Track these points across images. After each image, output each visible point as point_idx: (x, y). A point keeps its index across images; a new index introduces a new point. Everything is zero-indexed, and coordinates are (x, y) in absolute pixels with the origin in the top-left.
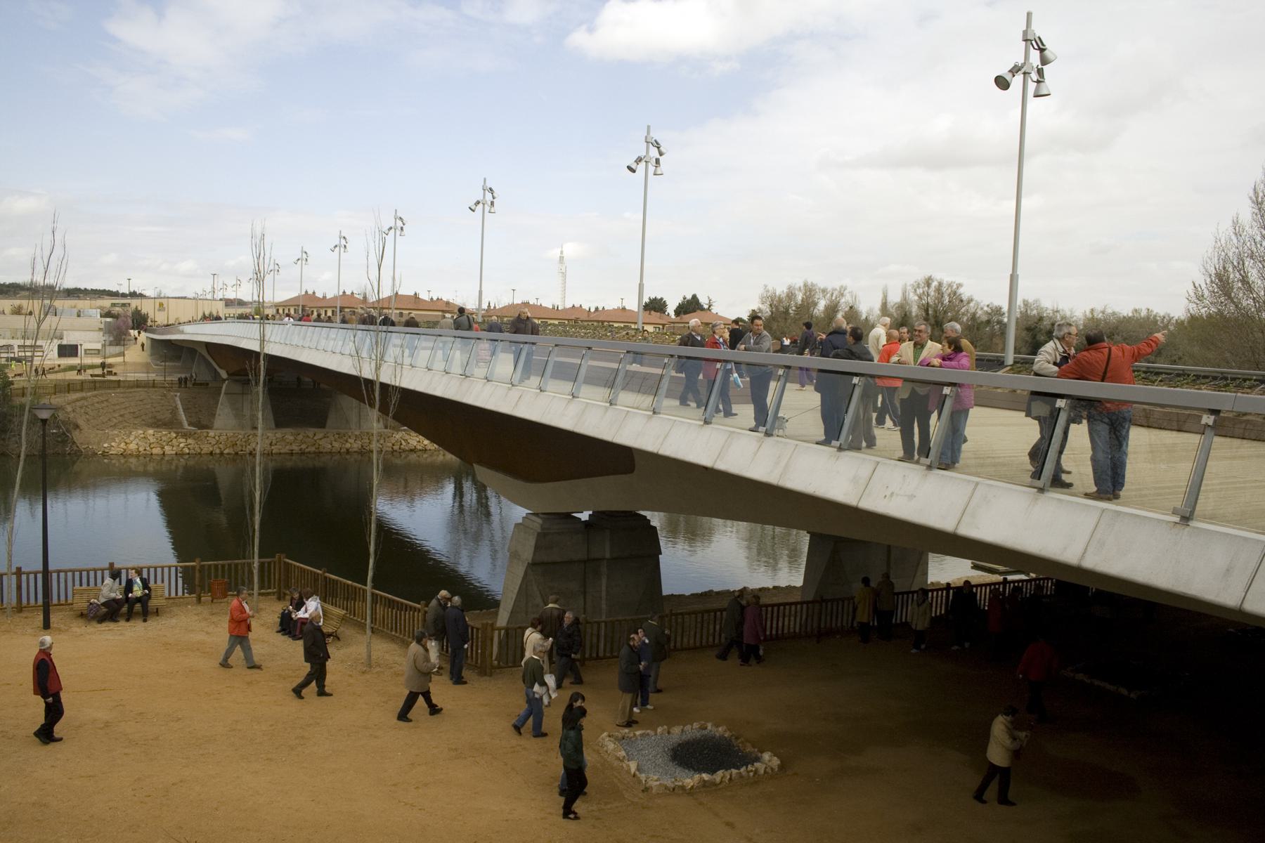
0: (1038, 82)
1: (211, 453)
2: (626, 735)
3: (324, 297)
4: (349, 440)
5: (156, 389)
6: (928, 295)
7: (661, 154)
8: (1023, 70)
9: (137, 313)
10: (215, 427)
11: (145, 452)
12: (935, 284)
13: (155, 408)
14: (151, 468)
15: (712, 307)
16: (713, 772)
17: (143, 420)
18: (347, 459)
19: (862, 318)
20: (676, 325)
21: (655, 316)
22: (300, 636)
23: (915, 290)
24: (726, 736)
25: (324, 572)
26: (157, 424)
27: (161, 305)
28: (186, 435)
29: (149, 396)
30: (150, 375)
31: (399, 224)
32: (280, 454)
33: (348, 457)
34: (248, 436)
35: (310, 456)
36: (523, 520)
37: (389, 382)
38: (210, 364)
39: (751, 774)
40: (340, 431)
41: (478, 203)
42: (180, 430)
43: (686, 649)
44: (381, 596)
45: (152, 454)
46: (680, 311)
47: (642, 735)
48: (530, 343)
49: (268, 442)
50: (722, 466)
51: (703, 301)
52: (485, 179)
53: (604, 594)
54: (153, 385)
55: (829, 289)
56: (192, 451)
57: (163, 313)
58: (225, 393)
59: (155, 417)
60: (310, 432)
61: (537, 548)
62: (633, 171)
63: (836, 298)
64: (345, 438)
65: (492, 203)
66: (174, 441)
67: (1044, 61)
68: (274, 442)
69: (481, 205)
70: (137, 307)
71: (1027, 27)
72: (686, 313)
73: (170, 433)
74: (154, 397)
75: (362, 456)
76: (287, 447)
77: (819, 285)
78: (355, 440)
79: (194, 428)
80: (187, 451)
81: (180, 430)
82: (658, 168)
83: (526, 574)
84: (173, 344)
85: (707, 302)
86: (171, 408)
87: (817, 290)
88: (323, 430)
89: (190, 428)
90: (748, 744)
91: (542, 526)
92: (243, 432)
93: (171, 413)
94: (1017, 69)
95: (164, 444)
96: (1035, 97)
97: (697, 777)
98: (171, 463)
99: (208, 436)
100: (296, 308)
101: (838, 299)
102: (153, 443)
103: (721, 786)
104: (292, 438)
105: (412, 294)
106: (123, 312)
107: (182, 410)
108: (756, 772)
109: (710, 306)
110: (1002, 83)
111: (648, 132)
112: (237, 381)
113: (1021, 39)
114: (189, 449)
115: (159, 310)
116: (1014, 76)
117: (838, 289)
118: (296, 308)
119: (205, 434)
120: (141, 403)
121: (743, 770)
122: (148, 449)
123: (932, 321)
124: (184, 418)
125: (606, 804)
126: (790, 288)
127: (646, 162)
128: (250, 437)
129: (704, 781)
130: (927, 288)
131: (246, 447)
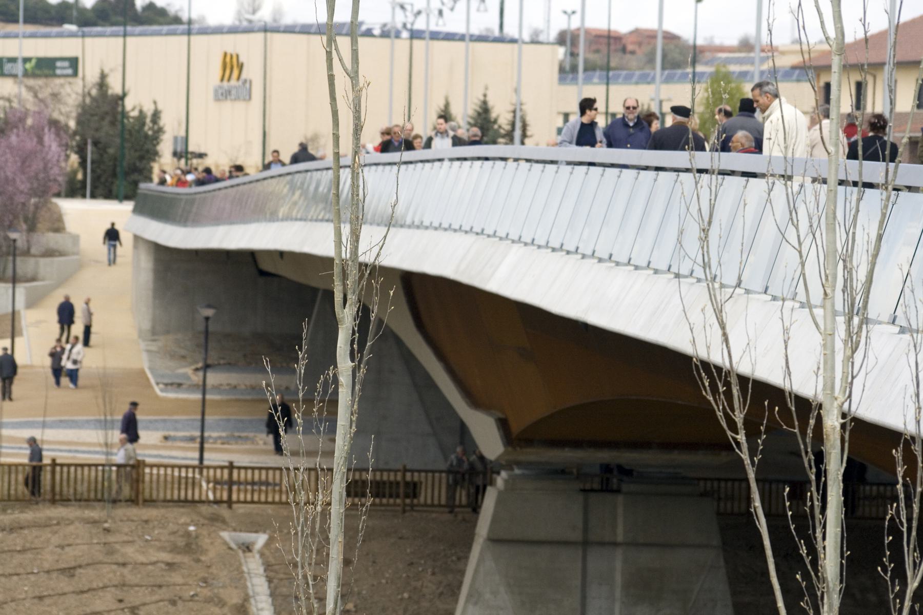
37: (687, 349)
38: (431, 385)
57: (240, 106)
58: (494, 540)
70: (103, 76)
74: (130, 552)
84: (263, 273)
106: (27, 96)
112: (560, 473)
115: (223, 95)
120: (64, 584)
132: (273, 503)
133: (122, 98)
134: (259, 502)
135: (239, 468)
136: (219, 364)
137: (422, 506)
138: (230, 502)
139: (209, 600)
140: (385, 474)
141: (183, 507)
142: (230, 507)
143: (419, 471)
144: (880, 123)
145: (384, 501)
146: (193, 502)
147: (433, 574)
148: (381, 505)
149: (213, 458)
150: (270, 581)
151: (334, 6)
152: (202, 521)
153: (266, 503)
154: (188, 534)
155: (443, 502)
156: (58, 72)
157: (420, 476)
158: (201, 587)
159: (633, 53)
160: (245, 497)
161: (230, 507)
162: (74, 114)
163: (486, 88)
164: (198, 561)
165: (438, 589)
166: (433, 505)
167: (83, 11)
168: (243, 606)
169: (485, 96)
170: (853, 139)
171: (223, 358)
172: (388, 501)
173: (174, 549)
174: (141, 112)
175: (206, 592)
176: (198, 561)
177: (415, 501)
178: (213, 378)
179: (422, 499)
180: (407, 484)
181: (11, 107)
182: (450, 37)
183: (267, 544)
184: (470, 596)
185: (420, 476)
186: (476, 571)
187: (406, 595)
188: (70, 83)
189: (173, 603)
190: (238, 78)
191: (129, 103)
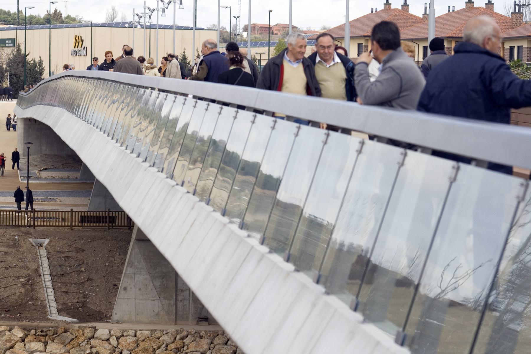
10: (115, 317)
19: (22, 53)
27: (79, 41)
34: (182, 339)
48: (219, 102)
57: (82, 58)
73: (10, 331)
79: (69, 319)
92: (172, 329)
93: (24, 285)
99: (93, 337)
107: (48, 277)
119: (88, 333)
124: (52, 297)
128: (186, 341)
132: (53, 226)
133: (25, 56)
134: (47, 226)
135: (38, 211)
136: (51, 168)
137: (117, 226)
138: (34, 226)
139: (22, 268)
140: (92, 213)
141: (14, 228)
142: (34, 228)
143: (115, 212)
144: (238, 58)
145: (101, 224)
146: (18, 226)
147: (120, 255)
148: (99, 226)
150: (49, 259)
152: (21, 234)
153: (50, 226)
154: (15, 240)
155: (126, 225)
156: (7, 45)
157: (115, 214)
158: (19, 262)
159: (276, 34)
160: (68, 224)
161: (34, 228)
162: (5, 63)
163: (185, 49)
164: (18, 251)
165: (121, 261)
166: (121, 226)
167: (39, 19)
168: (37, 269)
169: (184, 52)
171: (53, 166)
172: (93, 225)
173: (8, 246)
174: (34, 61)
175: (21, 264)
176: (18, 251)
177: (114, 224)
179: (117, 223)
180: (110, 217)
182: (165, 27)
183: (49, 244)
184: (129, 263)
185: (115, 214)
186: (131, 253)
187: (107, 264)
188: (3, 49)
189: (7, 269)
190: (81, 47)
191: (29, 58)
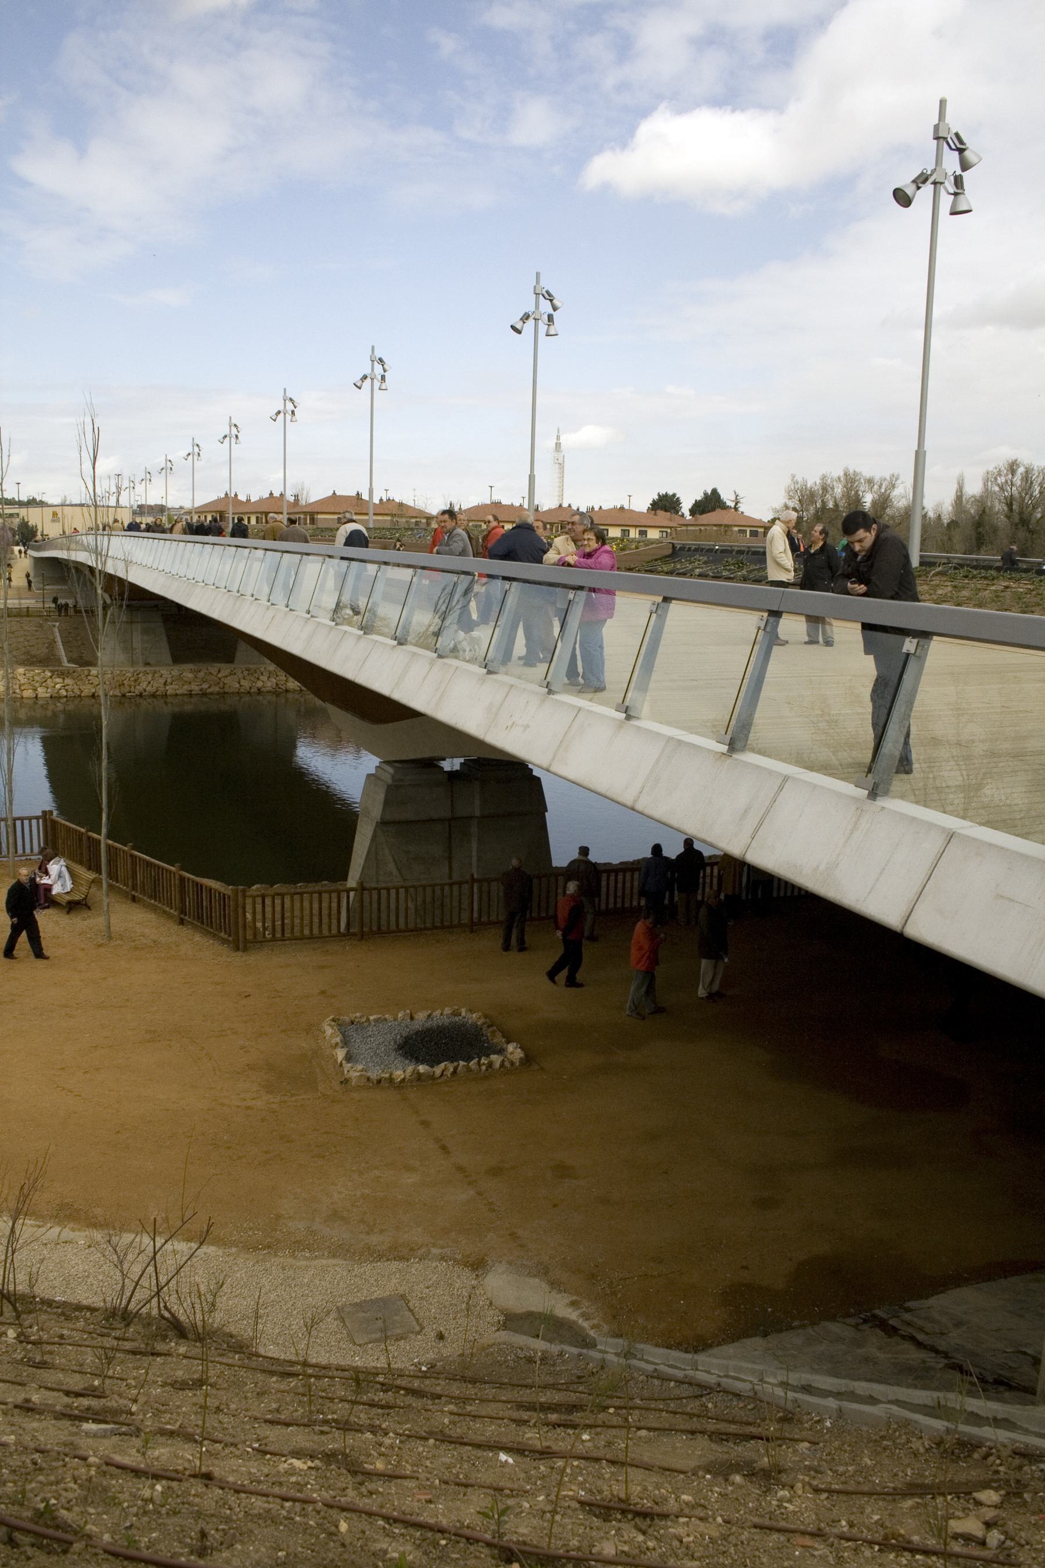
0: (956, 194)
1: (93, 696)
2: (357, 1020)
3: (248, 500)
4: (261, 677)
5: (31, 619)
6: (1012, 485)
7: (555, 309)
8: (931, 180)
9: (24, 524)
11: (14, 695)
12: (1021, 470)
13: (28, 641)
14: (22, 714)
15: (739, 505)
16: (433, 1063)
17: (15, 657)
18: (258, 701)
20: (690, 528)
21: (663, 517)
22: (47, 904)
23: (996, 479)
24: (479, 1023)
25: (88, 831)
26: (31, 661)
28: (63, 675)
29: (22, 627)
30: (23, 601)
31: (290, 406)
32: (176, 695)
33: (260, 698)
35: (211, 696)
36: (376, 770)
39: (484, 1068)
40: (251, 666)
41: (365, 377)
42: (57, 668)
43: (494, 923)
44: (140, 858)
45: (22, 698)
46: (698, 508)
47: (377, 1021)
49: (162, 681)
50: (396, 696)
51: (727, 497)
52: (373, 347)
53: (474, 860)
54: (27, 613)
55: (877, 479)
56: (70, 694)
59: (27, 653)
60: (214, 668)
61: (387, 803)
62: (519, 332)
63: (886, 491)
64: (256, 675)
65: (383, 378)
66: (49, 680)
67: (965, 166)
68: (169, 680)
69: (368, 380)
71: (940, 120)
72: (703, 512)
75: (277, 696)
76: (185, 687)
77: (864, 474)
78: (269, 677)
80: (64, 693)
81: (57, 668)
82: (552, 327)
83: (375, 831)
85: (733, 498)
86: (47, 641)
87: (862, 481)
88: (232, 666)
89: (69, 665)
90: (499, 1034)
91: (393, 777)
92: (131, 670)
94: (924, 177)
95: (37, 685)
96: (952, 214)
97: (410, 1069)
98: (47, 709)
99: (89, 675)
100: (259, 515)
101: (888, 492)
102: (24, 684)
103: (440, 1081)
104: (191, 675)
105: (354, 494)
107: (60, 643)
108: (490, 1065)
109: (736, 504)
110: (903, 198)
111: (538, 281)
113: (932, 136)
114: (67, 690)
115: (53, 521)
116: (919, 188)
117: (888, 478)
118: (259, 515)
119: (86, 672)
121: (473, 1063)
122: (18, 691)
123: (1016, 519)
124: (63, 653)
125: (292, 1095)
126: (824, 478)
127: (535, 319)
128: (140, 676)
129: (418, 1073)
130: (1010, 476)
131: (135, 687)
149: (46, 606)
151: (915, 630)
170: (138, 520)
178: (47, 587)
181: (945, 1561)
191: (29, 524)
